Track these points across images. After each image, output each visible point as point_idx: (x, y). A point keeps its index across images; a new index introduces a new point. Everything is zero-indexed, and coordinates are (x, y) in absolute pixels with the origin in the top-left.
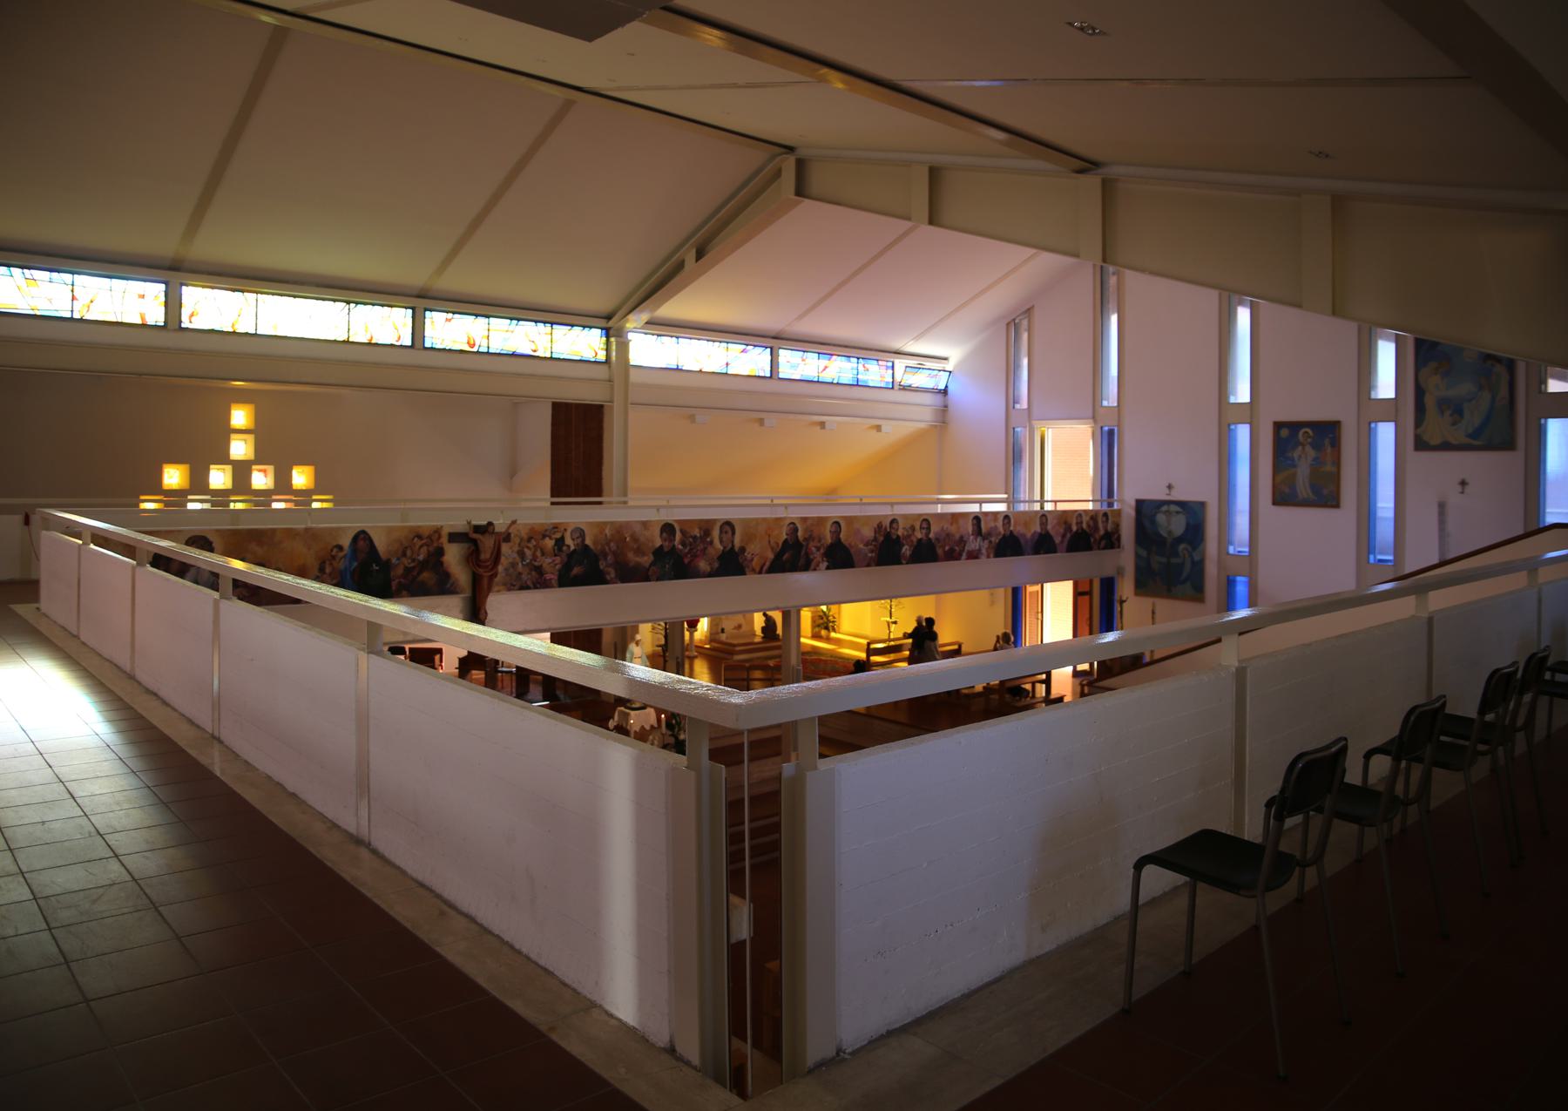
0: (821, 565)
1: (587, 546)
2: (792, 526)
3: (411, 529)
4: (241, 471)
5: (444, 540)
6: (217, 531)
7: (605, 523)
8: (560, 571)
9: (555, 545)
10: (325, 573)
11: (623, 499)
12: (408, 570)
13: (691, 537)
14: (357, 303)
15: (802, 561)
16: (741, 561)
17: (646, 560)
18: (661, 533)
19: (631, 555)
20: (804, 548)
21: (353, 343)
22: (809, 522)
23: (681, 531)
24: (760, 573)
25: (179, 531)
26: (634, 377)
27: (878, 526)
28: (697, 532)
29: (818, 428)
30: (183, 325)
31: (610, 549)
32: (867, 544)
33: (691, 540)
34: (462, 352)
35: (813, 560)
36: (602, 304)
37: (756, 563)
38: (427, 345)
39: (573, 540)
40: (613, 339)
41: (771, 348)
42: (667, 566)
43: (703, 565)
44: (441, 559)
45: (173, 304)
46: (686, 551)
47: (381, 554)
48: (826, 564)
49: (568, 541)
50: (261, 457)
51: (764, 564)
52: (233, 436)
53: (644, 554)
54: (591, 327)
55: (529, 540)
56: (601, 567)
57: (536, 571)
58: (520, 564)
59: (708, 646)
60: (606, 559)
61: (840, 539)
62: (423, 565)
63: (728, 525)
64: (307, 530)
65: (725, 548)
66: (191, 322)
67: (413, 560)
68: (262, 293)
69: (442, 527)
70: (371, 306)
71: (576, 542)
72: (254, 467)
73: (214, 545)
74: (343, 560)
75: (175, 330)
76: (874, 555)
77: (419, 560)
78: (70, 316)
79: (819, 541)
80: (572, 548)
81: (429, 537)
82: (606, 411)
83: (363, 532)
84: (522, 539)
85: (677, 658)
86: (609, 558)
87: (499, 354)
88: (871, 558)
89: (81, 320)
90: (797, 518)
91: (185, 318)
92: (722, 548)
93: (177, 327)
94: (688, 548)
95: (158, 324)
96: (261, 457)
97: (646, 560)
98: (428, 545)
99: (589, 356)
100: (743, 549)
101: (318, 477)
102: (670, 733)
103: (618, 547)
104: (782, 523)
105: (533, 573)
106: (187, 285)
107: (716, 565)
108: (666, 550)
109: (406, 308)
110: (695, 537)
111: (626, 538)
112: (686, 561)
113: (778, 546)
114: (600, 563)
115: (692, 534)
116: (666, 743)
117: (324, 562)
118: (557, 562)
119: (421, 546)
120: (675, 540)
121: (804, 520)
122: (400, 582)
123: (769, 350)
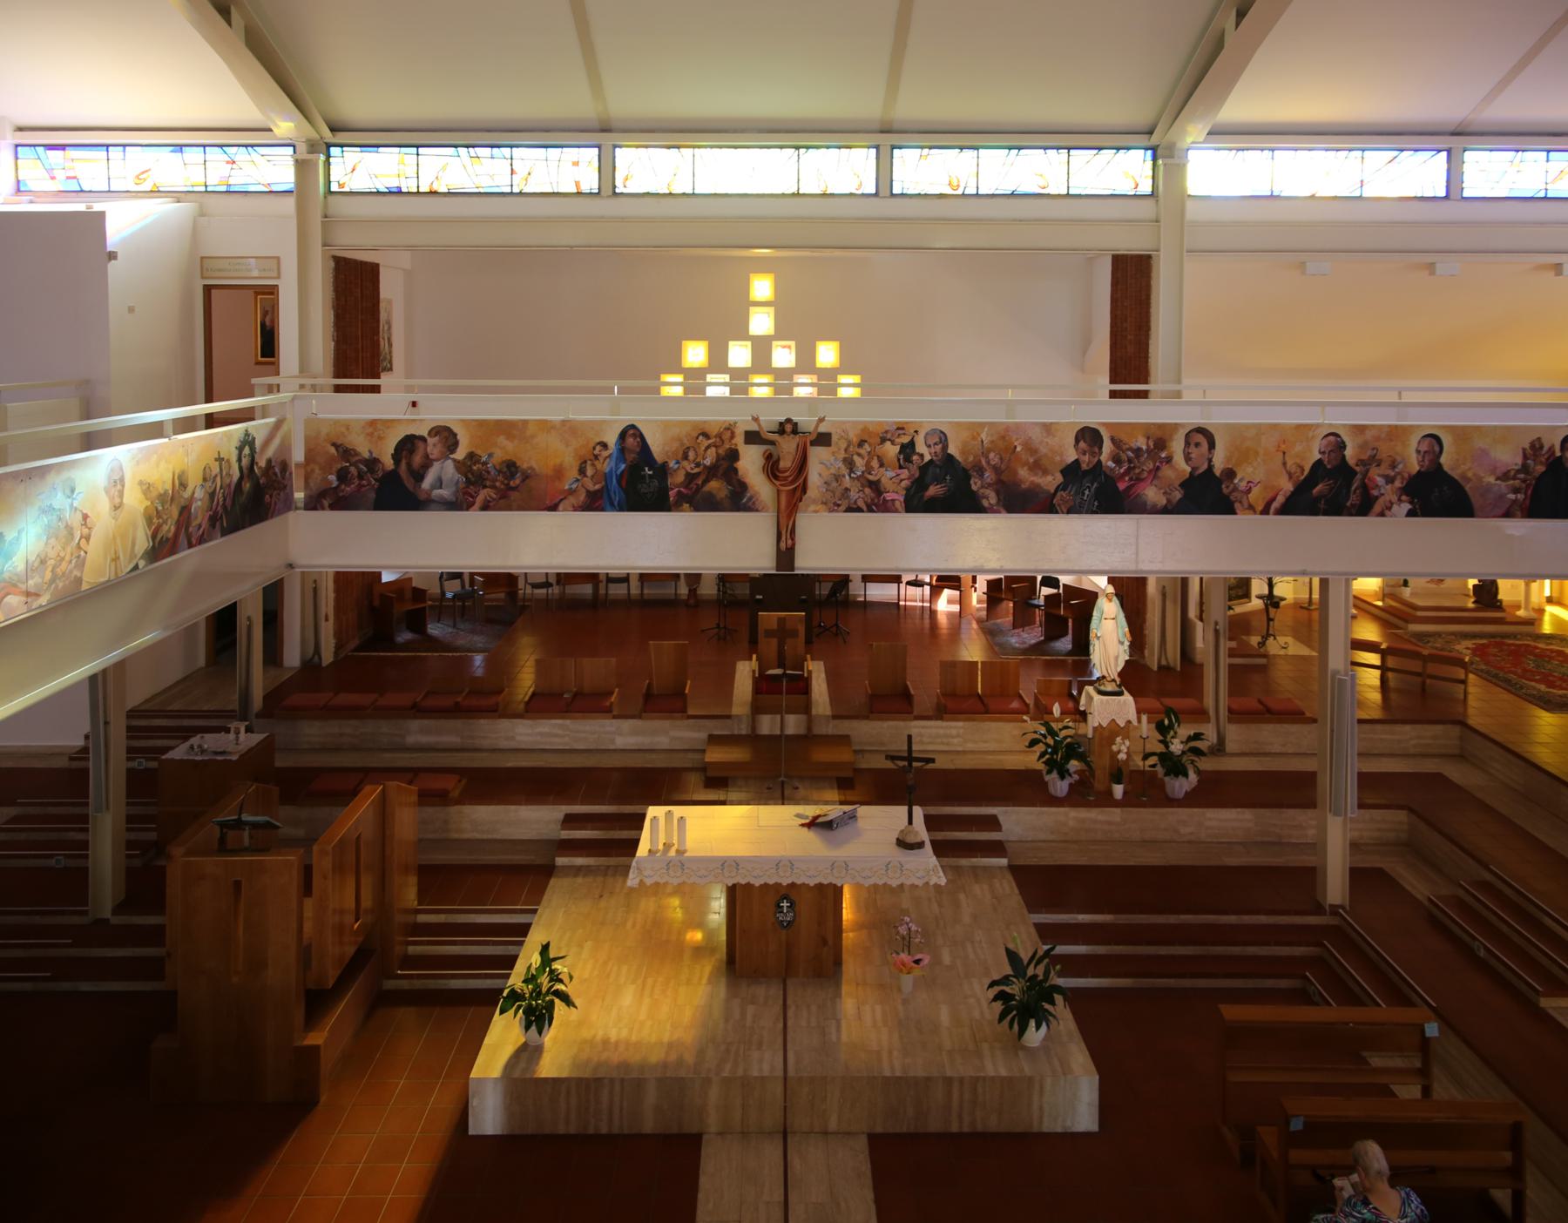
0: (1395, 507)
1: (950, 457)
2: (1331, 438)
3: (695, 424)
4: (762, 347)
5: (739, 440)
6: (463, 421)
7: (982, 425)
8: (908, 489)
9: (900, 453)
10: (585, 476)
11: (1176, 387)
12: (690, 477)
13: (1130, 449)
14: (808, 147)
15: (1354, 499)
16: (1225, 491)
17: (1051, 481)
18: (1077, 441)
19: (1023, 473)
20: (1359, 476)
21: (804, 195)
22: (1369, 435)
23: (1113, 439)
24: (1265, 511)
25: (421, 420)
26: (1193, 211)
27: (1532, 445)
28: (1141, 443)
29: (1553, 273)
30: (617, 191)
31: (988, 463)
32: (1505, 476)
33: (1130, 454)
34: (941, 196)
35: (1377, 498)
36: (1139, 115)
37: (1257, 497)
38: (895, 191)
39: (929, 446)
40: (1160, 162)
41: (1449, 151)
42: (1087, 492)
43: (1152, 494)
44: (735, 465)
45: (607, 169)
46: (1122, 471)
47: (655, 455)
48: (1406, 507)
49: (921, 447)
50: (781, 333)
51: (1273, 499)
52: (753, 310)
53: (1045, 472)
54: (1128, 149)
55: (861, 444)
56: (974, 488)
57: (870, 487)
58: (847, 477)
59: (1380, 603)
60: (982, 476)
61: (1440, 466)
62: (712, 472)
63: (1202, 436)
64: (564, 422)
65: (1194, 469)
66: (625, 186)
67: (698, 465)
68: (699, 147)
69: (735, 423)
70: (825, 150)
71: (933, 450)
72: (775, 343)
73: (458, 437)
74: (608, 460)
75: (1458, 200)
76: (1520, 496)
77: (705, 466)
78: (510, 191)
79: (1393, 466)
80: (927, 458)
81: (719, 436)
82: (1154, 262)
83: (633, 427)
84: (849, 443)
85: (1216, 623)
86: (987, 474)
87: (993, 196)
88: (1515, 501)
89: (521, 194)
90: (1344, 425)
91: (619, 183)
92: (1189, 469)
93: (611, 193)
94: (1126, 466)
95: (593, 191)
96: (781, 333)
97: (1051, 481)
98: (716, 447)
99: (1126, 188)
100: (1230, 474)
101: (843, 353)
102: (1161, 738)
103: (1001, 459)
104: (1311, 434)
105: (867, 490)
106: (620, 147)
107: (1178, 495)
108: (1084, 467)
109: (869, 147)
110: (1138, 451)
111: (1015, 447)
112: (1122, 486)
113: (1303, 470)
114: (972, 482)
115: (1134, 445)
116: (1147, 751)
117: (585, 462)
118: (902, 477)
119: (708, 448)
120: (1101, 453)
121: (1360, 429)
122: (679, 491)
123: (1444, 154)
